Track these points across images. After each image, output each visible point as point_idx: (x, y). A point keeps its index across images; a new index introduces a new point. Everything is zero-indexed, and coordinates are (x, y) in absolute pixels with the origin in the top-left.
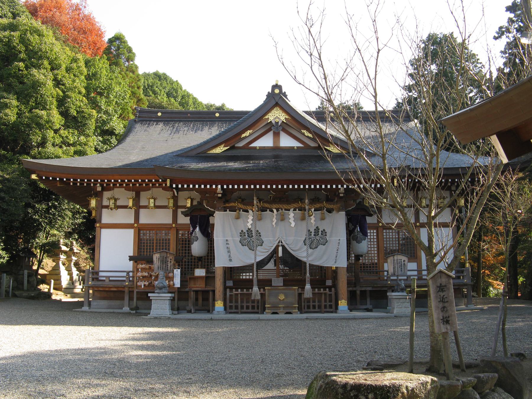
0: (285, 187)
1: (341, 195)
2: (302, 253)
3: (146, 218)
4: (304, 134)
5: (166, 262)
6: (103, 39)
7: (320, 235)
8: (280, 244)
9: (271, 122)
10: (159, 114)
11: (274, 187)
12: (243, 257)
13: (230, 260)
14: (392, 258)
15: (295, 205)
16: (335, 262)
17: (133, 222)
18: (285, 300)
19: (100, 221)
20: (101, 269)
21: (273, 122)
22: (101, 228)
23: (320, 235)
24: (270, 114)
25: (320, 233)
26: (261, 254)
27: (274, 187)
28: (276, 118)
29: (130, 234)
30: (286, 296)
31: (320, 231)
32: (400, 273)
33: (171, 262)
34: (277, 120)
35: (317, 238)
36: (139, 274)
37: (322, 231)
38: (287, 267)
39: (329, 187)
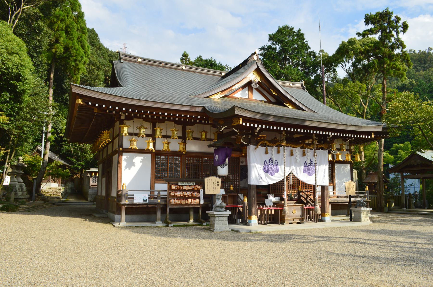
33: (218, 185)
36: (172, 194)
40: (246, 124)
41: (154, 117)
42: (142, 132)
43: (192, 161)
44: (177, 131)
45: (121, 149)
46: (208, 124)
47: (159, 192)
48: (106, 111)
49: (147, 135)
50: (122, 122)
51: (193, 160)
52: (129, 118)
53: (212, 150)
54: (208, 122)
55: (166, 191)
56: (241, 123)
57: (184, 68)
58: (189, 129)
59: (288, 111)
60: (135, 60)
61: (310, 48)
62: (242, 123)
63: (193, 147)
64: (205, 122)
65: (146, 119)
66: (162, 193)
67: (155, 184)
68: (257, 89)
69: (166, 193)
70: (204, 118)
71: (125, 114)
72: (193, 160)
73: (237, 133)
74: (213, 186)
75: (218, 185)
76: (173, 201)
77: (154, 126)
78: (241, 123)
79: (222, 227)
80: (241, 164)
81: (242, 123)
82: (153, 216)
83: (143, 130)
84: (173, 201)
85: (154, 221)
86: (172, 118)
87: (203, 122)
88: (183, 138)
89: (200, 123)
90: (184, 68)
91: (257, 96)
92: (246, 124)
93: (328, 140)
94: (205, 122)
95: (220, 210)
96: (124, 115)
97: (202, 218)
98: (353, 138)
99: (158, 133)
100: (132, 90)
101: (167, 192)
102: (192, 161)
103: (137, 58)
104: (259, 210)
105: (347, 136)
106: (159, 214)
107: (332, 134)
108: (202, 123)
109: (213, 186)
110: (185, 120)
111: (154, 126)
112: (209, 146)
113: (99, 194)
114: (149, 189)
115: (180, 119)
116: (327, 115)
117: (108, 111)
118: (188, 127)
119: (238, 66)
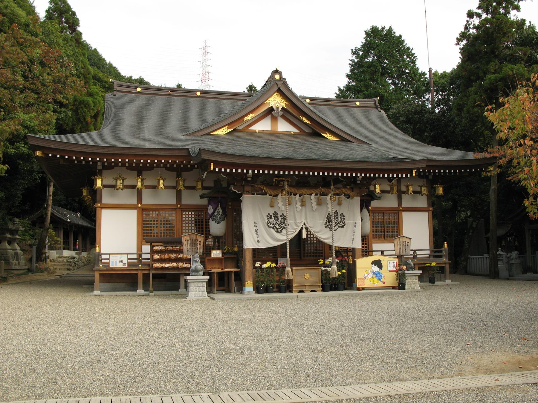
0: (306, 173)
1: (249, 179)
2: (324, 235)
3: (148, 199)
4: (302, 121)
5: (196, 244)
6: (420, 71)
7: (280, 219)
8: (304, 226)
9: (272, 107)
10: (139, 89)
11: (297, 173)
12: (270, 239)
13: (259, 242)
14: (398, 240)
15: (318, 191)
16: (352, 244)
17: (175, 203)
18: (310, 279)
19: (100, 202)
20: (102, 252)
21: (274, 107)
22: (102, 208)
23: (280, 219)
24: (271, 99)
25: (280, 218)
26: (283, 238)
27: (297, 173)
28: (276, 103)
29: (132, 215)
30: (311, 276)
31: (279, 216)
32: (404, 253)
33: (200, 244)
34: (278, 105)
35: (335, 221)
36: (156, 256)
37: (281, 216)
38: (443, 244)
39: (302, 173)
41: (139, 164)
43: (151, 216)
45: (401, 208)
47: (415, 251)
57: (358, 103)
60: (194, 95)
76: (157, 265)
79: (198, 294)
84: (157, 265)
85: (445, 279)
90: (358, 103)
91: (284, 127)
95: (196, 274)
100: (123, 130)
101: (149, 255)
103: (195, 91)
107: (361, 175)
111: (178, 176)
114: (136, 252)
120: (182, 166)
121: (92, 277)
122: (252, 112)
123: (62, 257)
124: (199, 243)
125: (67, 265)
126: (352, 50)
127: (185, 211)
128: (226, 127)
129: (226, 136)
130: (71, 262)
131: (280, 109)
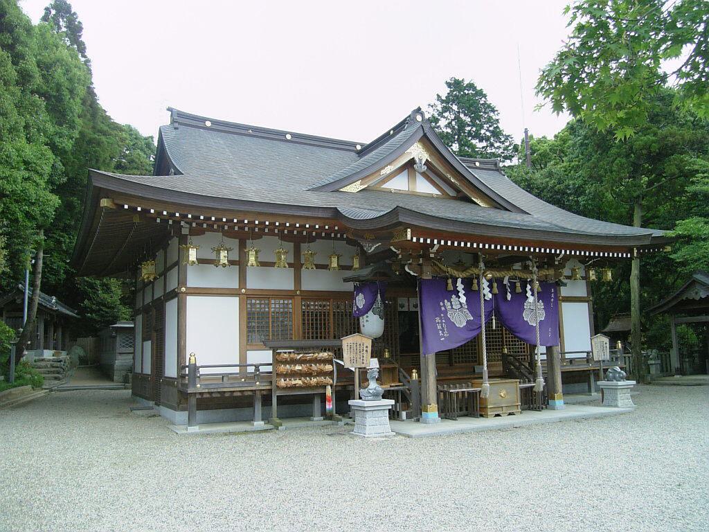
33: (367, 351)
40: (418, 239)
41: (242, 226)
42: (222, 257)
44: (286, 253)
45: (183, 289)
46: (342, 238)
47: (257, 367)
48: (156, 220)
49: (232, 263)
50: (183, 240)
51: (261, 304)
52: (198, 231)
53: (350, 287)
54: (342, 236)
55: (270, 364)
56: (409, 237)
58: (306, 249)
59: (480, 212)
60: (201, 124)
61: (466, 99)
62: (412, 238)
63: (315, 282)
64: (336, 235)
65: (230, 234)
66: (262, 369)
67: (248, 352)
68: (424, 174)
69: (270, 369)
70: (336, 228)
71: (191, 225)
72: (261, 304)
73: (398, 255)
74: (357, 352)
75: (367, 351)
76: (282, 383)
77: (242, 245)
78: (409, 237)
80: (400, 309)
81: (412, 238)
82: (247, 411)
83: (223, 254)
84: (282, 383)
85: (250, 420)
86: (276, 231)
87: (333, 235)
88: (296, 266)
89: (328, 236)
91: (424, 187)
92: (418, 239)
93: (557, 263)
94: (336, 235)
96: (188, 226)
97: (336, 413)
98: (597, 257)
99: (252, 259)
102: (312, 307)
103: (204, 120)
104: (442, 394)
105: (587, 254)
106: (258, 407)
108: (331, 238)
109: (357, 352)
110: (242, 228)
111: (242, 245)
112: (346, 280)
113: (138, 370)
115: (242, 228)
116: (545, 217)
117: (158, 220)
118: (304, 246)
119: (247, 128)
120: (302, 233)
121: (159, 392)
122: (390, 164)
123: (43, 360)
124: (365, 349)
125: (54, 372)
126: (447, 83)
127: (275, 299)
128: (359, 182)
129: (359, 195)
130: (57, 367)
131: (423, 162)
